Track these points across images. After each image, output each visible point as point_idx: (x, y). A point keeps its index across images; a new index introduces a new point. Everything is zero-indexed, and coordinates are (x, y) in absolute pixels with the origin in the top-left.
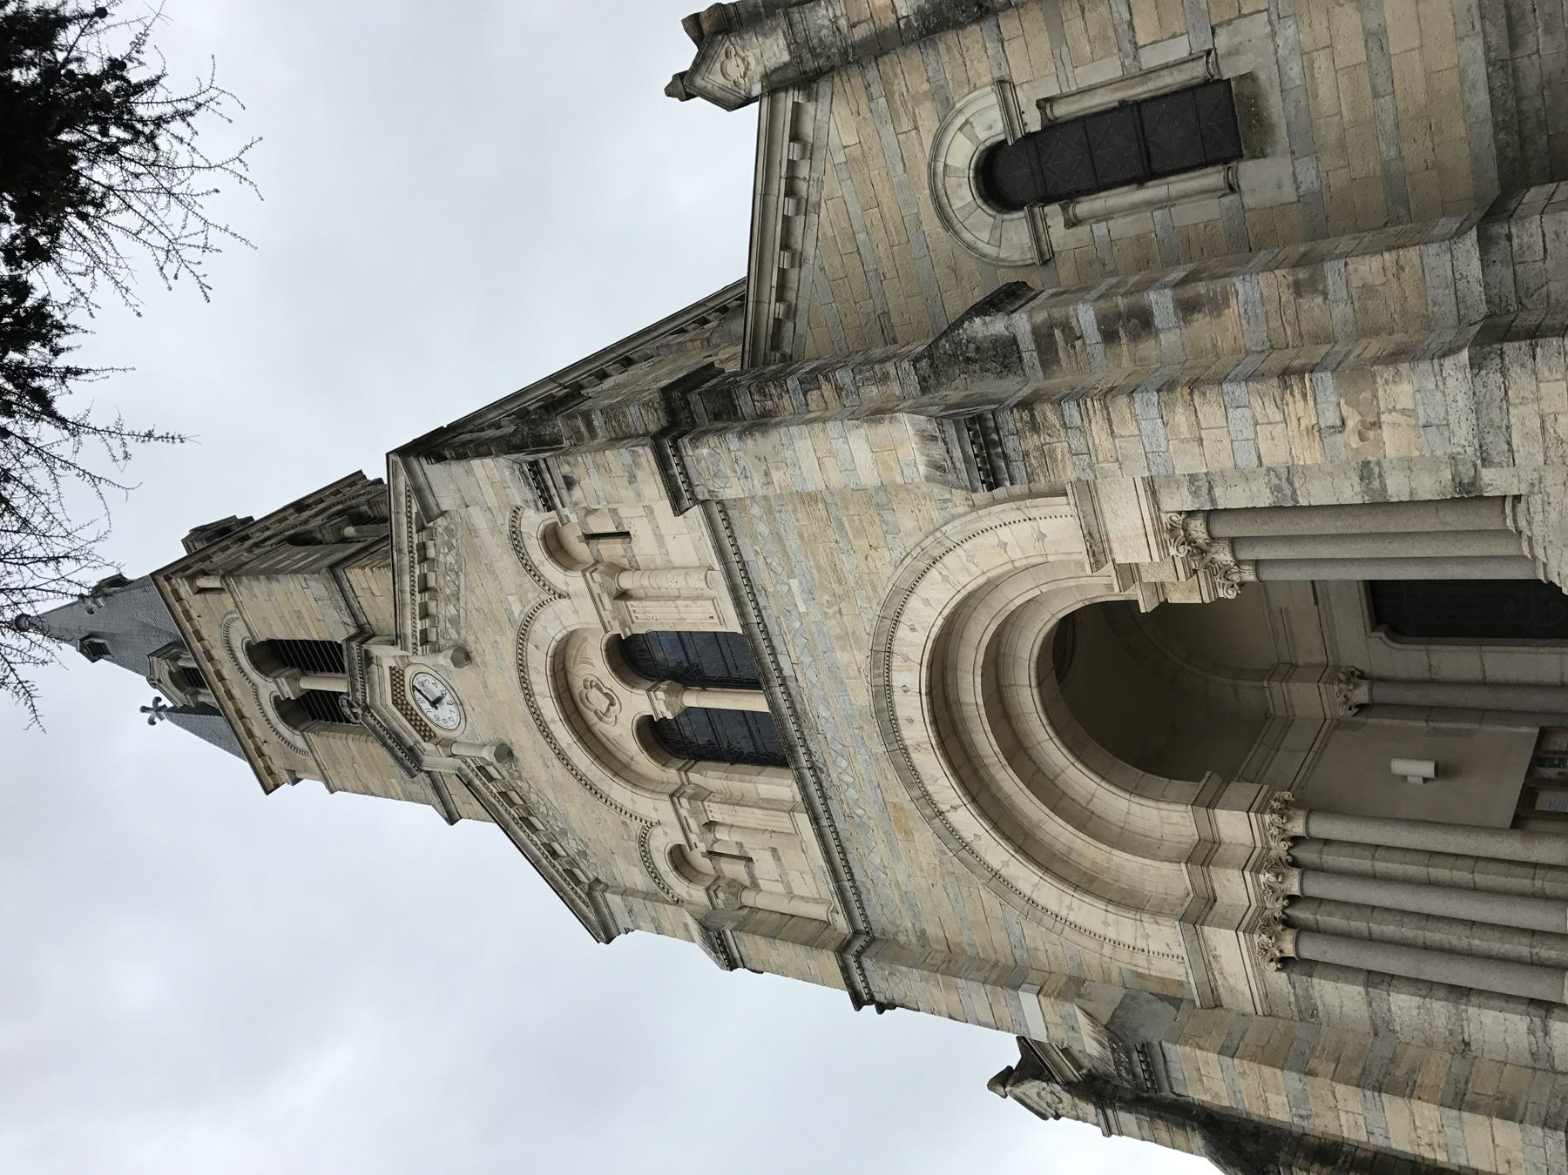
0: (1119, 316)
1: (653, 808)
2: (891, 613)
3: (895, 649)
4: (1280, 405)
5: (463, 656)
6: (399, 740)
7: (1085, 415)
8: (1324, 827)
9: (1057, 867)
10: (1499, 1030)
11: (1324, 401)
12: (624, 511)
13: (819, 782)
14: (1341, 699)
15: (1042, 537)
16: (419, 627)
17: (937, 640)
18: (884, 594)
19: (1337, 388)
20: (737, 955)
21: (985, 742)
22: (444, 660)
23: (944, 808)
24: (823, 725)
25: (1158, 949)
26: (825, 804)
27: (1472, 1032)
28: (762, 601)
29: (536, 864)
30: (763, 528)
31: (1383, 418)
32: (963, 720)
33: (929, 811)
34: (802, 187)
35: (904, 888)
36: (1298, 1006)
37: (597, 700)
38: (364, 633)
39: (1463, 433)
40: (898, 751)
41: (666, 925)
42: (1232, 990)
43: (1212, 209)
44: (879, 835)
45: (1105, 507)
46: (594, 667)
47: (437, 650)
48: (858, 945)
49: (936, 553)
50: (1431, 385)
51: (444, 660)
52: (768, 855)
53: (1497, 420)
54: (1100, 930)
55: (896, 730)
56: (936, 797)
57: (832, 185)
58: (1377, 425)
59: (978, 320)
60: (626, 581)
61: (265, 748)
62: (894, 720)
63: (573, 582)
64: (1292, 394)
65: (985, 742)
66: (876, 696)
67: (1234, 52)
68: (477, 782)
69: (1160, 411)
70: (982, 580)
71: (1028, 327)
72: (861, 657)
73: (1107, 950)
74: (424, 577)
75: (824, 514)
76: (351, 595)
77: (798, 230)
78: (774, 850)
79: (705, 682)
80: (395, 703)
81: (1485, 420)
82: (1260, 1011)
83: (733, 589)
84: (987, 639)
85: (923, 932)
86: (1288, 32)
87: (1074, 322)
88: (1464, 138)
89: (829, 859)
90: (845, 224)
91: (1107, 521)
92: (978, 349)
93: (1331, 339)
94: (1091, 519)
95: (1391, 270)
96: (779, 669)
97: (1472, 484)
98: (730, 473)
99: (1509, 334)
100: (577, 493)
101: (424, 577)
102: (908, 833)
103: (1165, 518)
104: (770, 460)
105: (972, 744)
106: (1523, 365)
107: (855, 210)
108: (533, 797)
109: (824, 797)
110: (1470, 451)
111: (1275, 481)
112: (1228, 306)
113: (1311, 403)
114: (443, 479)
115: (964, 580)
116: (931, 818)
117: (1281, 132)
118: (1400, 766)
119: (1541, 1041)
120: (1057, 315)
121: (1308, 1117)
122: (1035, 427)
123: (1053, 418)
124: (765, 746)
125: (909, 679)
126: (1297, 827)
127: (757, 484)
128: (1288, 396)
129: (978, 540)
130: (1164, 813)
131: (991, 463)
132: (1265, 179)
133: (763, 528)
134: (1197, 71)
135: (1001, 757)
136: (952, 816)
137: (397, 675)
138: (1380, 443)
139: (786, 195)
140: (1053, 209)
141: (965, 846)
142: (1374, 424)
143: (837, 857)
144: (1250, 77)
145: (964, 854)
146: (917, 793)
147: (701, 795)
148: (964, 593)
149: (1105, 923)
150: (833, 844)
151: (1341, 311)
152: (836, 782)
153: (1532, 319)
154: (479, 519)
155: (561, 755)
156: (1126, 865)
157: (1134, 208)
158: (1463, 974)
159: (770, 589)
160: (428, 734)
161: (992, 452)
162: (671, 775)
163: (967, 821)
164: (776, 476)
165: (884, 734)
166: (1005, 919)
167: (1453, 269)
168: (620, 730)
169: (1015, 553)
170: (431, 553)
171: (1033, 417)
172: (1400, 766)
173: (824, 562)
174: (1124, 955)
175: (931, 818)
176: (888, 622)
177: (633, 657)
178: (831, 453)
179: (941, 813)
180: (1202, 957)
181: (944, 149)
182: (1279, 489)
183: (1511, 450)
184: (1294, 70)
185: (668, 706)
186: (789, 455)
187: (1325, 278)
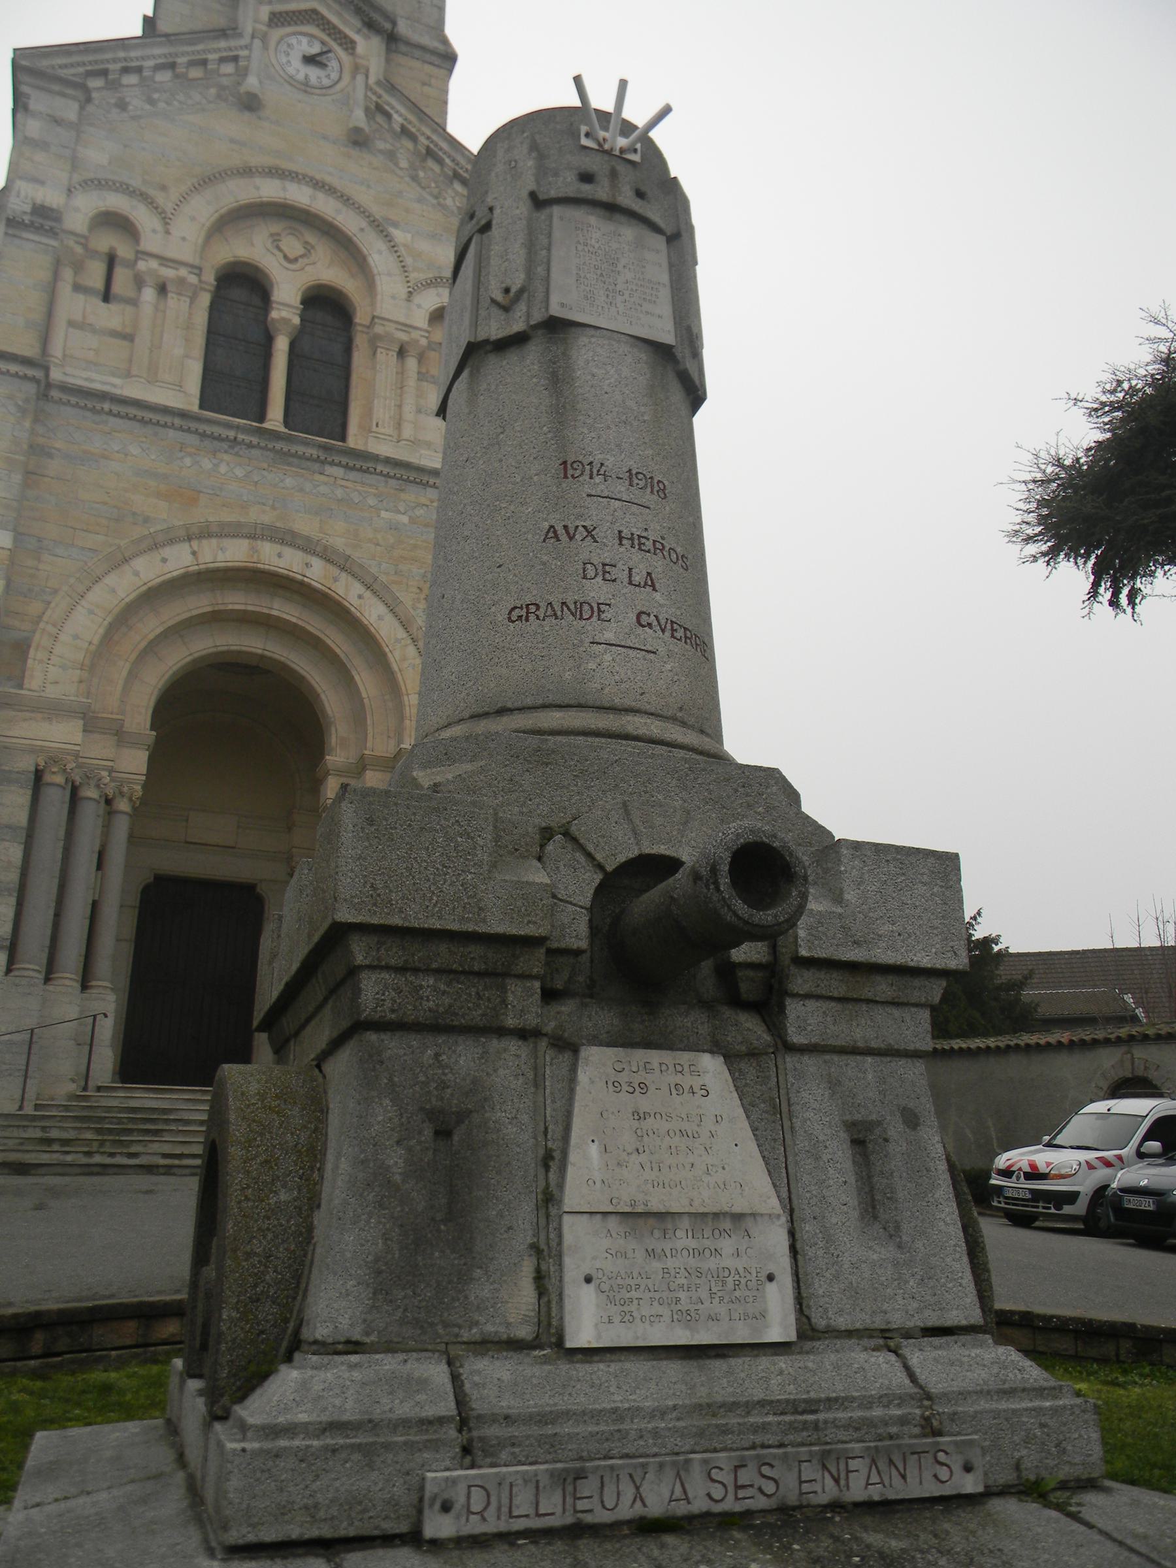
1: (182, 239)
3: (344, 575)
5: (358, 140)
13: (219, 438)
16: (395, 116)
17: (348, 612)
18: (394, 588)
20: (25, 235)
21: (236, 600)
23: (195, 544)
26: (196, 432)
28: (392, 482)
37: (292, 246)
40: (255, 534)
46: (326, 270)
51: (359, 118)
52: (115, 323)
55: (272, 539)
60: (412, 363)
62: (283, 542)
63: (420, 319)
65: (236, 600)
66: (308, 539)
68: (223, 44)
70: (395, 667)
72: (339, 543)
74: (440, 162)
76: (428, 57)
80: (314, 11)
83: (407, 466)
84: (329, 642)
85: (50, 456)
96: (332, 463)
101: (440, 162)
109: (203, 435)
115: (397, 654)
124: (232, 383)
125: (349, 591)
126: (123, 805)
137: (349, 45)
141: (156, 546)
143: (140, 413)
150: (155, 417)
162: (210, 278)
163: (179, 559)
168: (255, 247)
177: (326, 305)
180: (54, 710)
185: (286, 321)
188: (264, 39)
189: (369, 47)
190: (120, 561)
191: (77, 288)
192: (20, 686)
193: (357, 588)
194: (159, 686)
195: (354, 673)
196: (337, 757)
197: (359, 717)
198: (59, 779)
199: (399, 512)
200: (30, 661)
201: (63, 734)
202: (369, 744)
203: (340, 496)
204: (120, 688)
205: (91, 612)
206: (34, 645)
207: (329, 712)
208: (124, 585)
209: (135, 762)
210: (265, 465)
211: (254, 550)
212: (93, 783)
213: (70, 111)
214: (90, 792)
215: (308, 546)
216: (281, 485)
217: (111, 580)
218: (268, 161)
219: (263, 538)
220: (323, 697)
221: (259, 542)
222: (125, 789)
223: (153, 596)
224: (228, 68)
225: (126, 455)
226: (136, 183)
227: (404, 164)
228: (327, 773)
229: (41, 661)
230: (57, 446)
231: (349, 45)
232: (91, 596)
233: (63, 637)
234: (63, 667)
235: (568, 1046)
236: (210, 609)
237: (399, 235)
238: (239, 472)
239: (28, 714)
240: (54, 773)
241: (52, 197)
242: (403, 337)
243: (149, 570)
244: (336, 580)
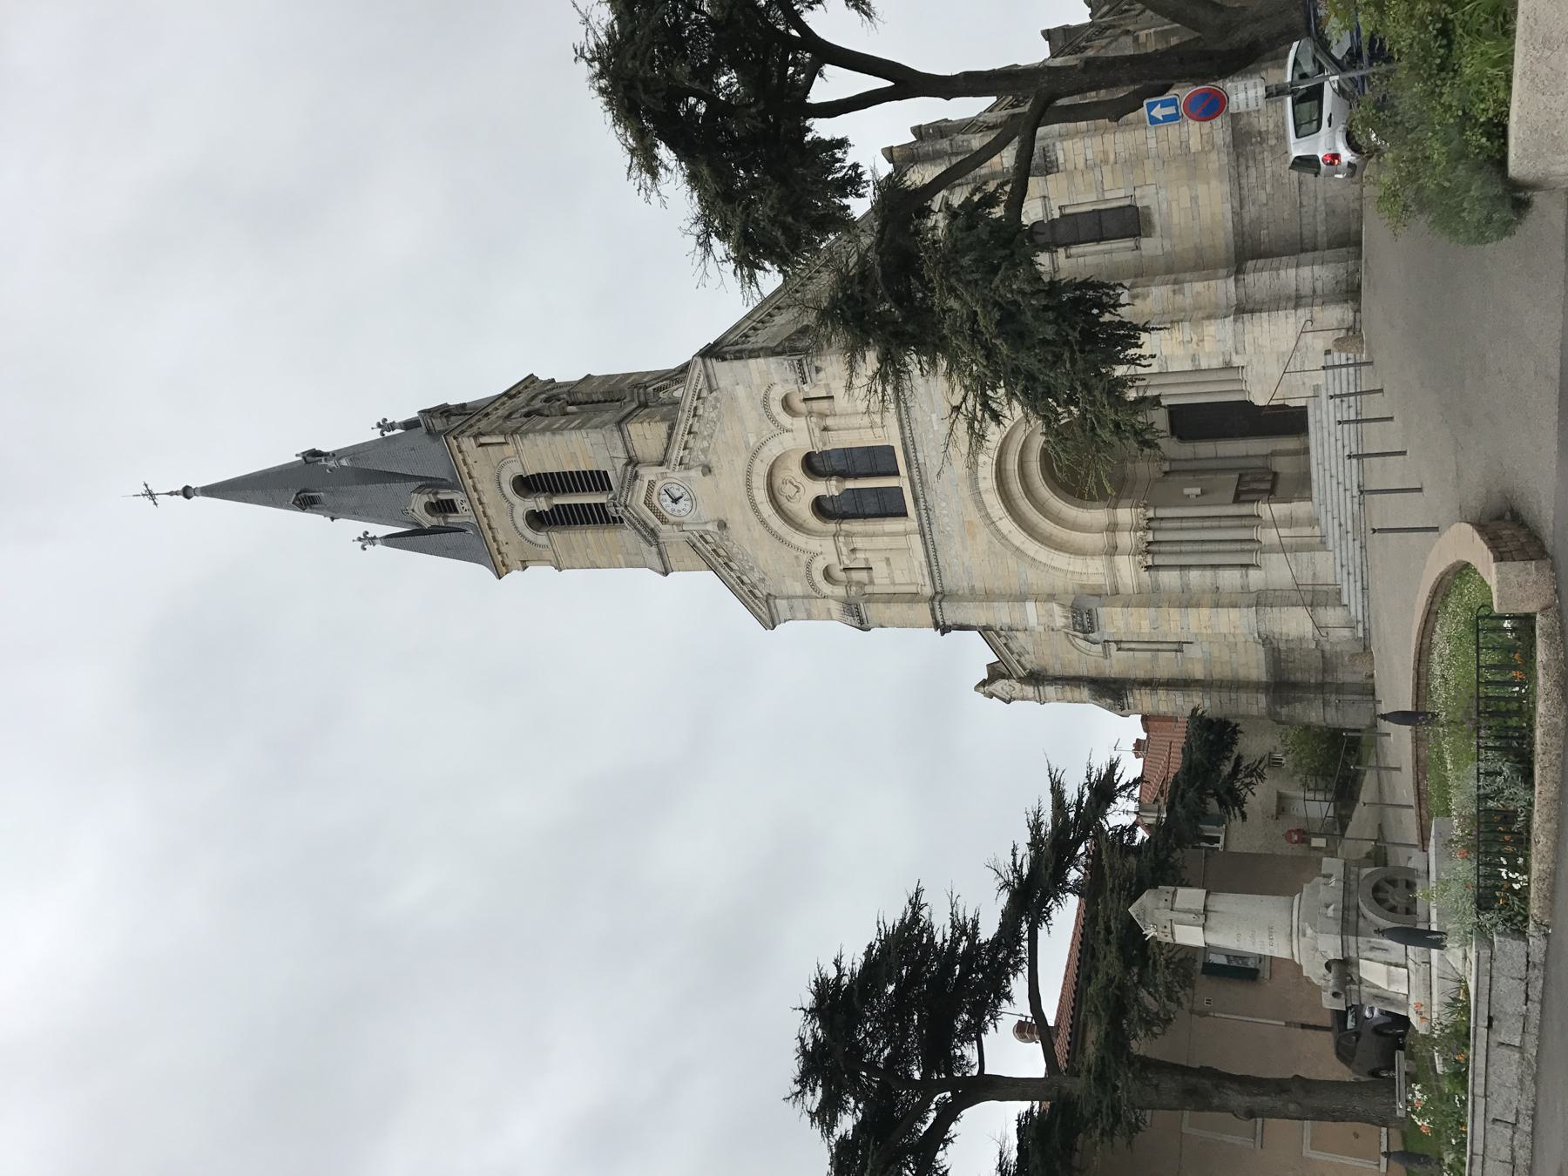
1: (823, 546)
5: (707, 470)
6: (645, 525)
8: (1162, 513)
10: (1230, 579)
12: (833, 385)
21: (1016, 487)
22: (695, 473)
25: (1093, 571)
27: (1221, 583)
29: (732, 589)
37: (789, 490)
38: (632, 462)
39: (1230, 343)
41: (815, 611)
43: (1129, 256)
46: (795, 470)
47: (688, 468)
48: (938, 597)
52: (883, 564)
60: (830, 422)
61: (503, 549)
63: (800, 423)
65: (1016, 487)
67: (1142, 197)
78: (888, 559)
79: (856, 476)
86: (1162, 192)
88: (1223, 237)
89: (928, 556)
93: (1184, 310)
99: (1244, 311)
100: (822, 375)
102: (973, 536)
108: (735, 550)
114: (724, 371)
117: (1158, 229)
118: (1187, 491)
124: (889, 506)
126: (1151, 514)
132: (1150, 246)
134: (1127, 202)
137: (651, 484)
140: (1061, 251)
141: (1004, 537)
144: (1147, 207)
147: (849, 535)
151: (1189, 301)
153: (1250, 306)
154: (741, 391)
155: (763, 522)
156: (1077, 537)
157: (1092, 254)
158: (1216, 560)
160: (664, 521)
162: (832, 526)
163: (1007, 525)
167: (1223, 289)
168: (802, 508)
170: (700, 412)
172: (1187, 491)
174: (1077, 577)
177: (813, 465)
180: (1113, 570)
184: (1164, 206)
188: (679, 524)
189: (648, 474)
190: (1018, 551)
191: (871, 582)
208: (1032, 548)
213: (782, 604)
218: (751, 515)
224: (708, 538)
226: (803, 570)
227: (705, 444)
231: (651, 484)
235: (1361, 980)
237: (752, 440)
241: (835, 607)
242: (817, 432)
243: (1018, 537)
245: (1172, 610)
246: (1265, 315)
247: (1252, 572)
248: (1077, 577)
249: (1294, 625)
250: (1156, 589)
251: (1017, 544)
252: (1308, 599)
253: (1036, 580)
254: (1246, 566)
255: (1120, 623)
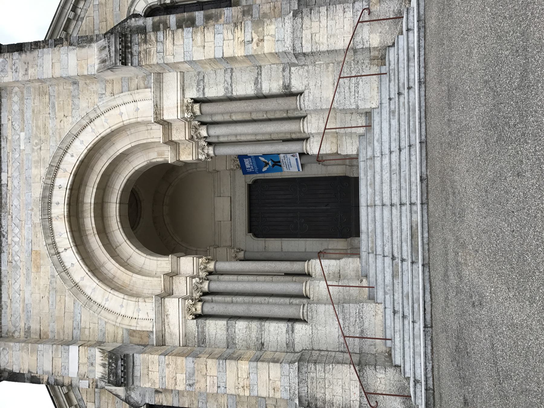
0: (184, 20)
2: (64, 146)
3: (61, 166)
4: (233, 32)
7: (165, 37)
9: (106, 282)
10: (275, 332)
11: (248, 32)
14: (234, 255)
15: (137, 109)
17: (82, 162)
19: (252, 27)
21: (89, 222)
23: (60, 250)
24: (14, 211)
25: (139, 315)
27: (266, 338)
30: (16, 108)
31: (265, 38)
32: (82, 212)
33: (53, 251)
34: (79, 11)
35: (26, 302)
36: (198, 338)
42: (171, 334)
44: (23, 271)
45: (165, 95)
49: (92, 116)
50: (281, 26)
53: (299, 35)
54: (118, 310)
55: (49, 209)
56: (58, 245)
57: (90, 11)
58: (263, 40)
59: (133, 19)
62: (50, 203)
64: (237, 29)
65: (89, 222)
66: (45, 189)
69: (192, 35)
70: (109, 131)
71: (151, 23)
72: (43, 171)
73: (120, 318)
75: (47, 100)
77: (72, 27)
81: (295, 35)
82: (181, 345)
84: (103, 169)
85: (29, 328)
87: (168, 21)
90: (91, 26)
91: (164, 101)
92: (131, 31)
94: (158, 99)
95: (272, 8)
97: (288, 86)
98: (9, 70)
102: (38, 267)
103: (185, 101)
104: (30, 64)
105: (83, 225)
106: (308, 16)
107: (97, 21)
110: (290, 48)
111: (226, 85)
112: (221, 18)
113: (243, 32)
116: (53, 255)
119: (290, 336)
120: (163, 19)
121: (193, 384)
122: (145, 41)
123: (153, 38)
125: (70, 163)
126: (211, 266)
127: (20, 75)
128: (236, 30)
129: (111, 112)
130: (159, 262)
131: (125, 55)
133: (16, 108)
135: (95, 229)
136: (64, 255)
138: (263, 47)
139: (71, 10)
141: (66, 270)
142: (262, 40)
145: (64, 274)
146: (50, 241)
148: (99, 137)
149: (122, 306)
152: (9, 242)
158: (263, 311)
159: (9, 138)
161: (127, 51)
163: (71, 257)
164: (31, 71)
165: (43, 210)
166: (74, 312)
169: (125, 117)
171: (146, 37)
173: (40, 123)
174: (126, 321)
175: (53, 255)
176: (62, 151)
178: (59, 61)
179: (59, 253)
180: (161, 315)
181: (135, 4)
182: (227, 89)
183: (302, 46)
186: (39, 61)
187: (252, 10)
192: (152, 332)
193: (67, 158)
194: (145, 255)
195: (118, 154)
196: (169, 156)
197: (145, 147)
198: (199, 306)
199: (19, 138)
200: (138, 329)
201: (174, 307)
202: (157, 140)
203: (18, 174)
204: (147, 278)
205: (107, 300)
206: (129, 328)
207: (145, 164)
209: (188, 264)
210: (10, 217)
211: (58, 217)
212: (199, 286)
214: (205, 286)
215: (49, 188)
216: (18, 207)
217: (88, 292)
219: (49, 214)
220: (137, 168)
221: (53, 216)
222: (202, 267)
223: (94, 268)
225: (20, 290)
228: (179, 161)
229: (137, 323)
230: (23, 325)
232: (99, 301)
233: (123, 313)
234: (139, 310)
236: (97, 236)
238: (17, 230)
239: (166, 326)
240: (196, 309)
243: (79, 271)
244: (65, 171)
245: (210, 362)
246: (323, 9)
247: (298, 326)
248: (126, 321)
249: (338, 390)
250: (202, 341)
251: (77, 279)
252: (356, 359)
253: (89, 322)
254: (293, 320)
255: (155, 376)
